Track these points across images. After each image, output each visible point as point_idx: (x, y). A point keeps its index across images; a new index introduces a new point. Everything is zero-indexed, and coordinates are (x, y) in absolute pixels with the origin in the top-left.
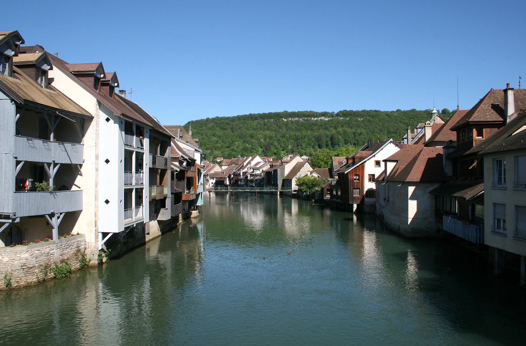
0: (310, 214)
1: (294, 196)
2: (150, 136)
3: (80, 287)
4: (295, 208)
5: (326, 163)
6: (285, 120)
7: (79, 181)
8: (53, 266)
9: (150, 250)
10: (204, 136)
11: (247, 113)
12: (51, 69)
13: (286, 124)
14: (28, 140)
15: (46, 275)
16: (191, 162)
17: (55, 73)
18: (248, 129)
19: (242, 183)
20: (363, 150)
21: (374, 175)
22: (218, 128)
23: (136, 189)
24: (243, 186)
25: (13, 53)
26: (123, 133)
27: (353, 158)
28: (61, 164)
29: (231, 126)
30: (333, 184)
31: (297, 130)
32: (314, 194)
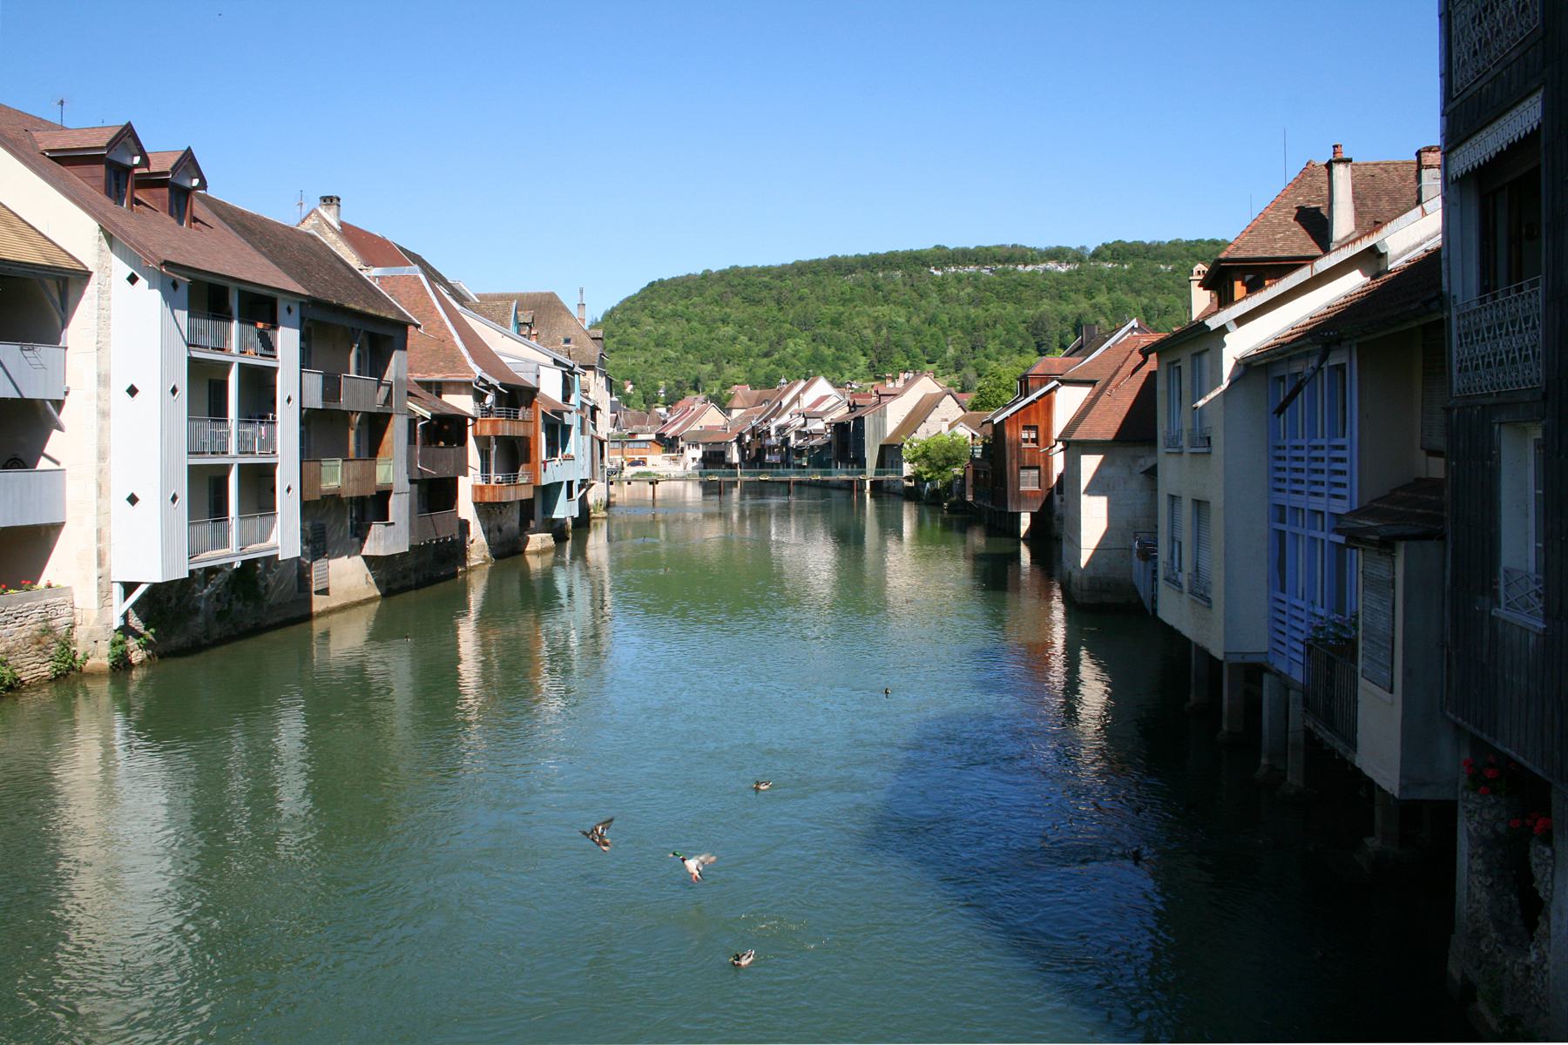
1: (912, 495)
2: (302, 319)
3: (56, 724)
6: (939, 273)
7: (55, 444)
9: (333, 637)
10: (695, 324)
11: (825, 255)
13: (941, 285)
18: (826, 300)
19: (775, 459)
22: (736, 299)
23: (240, 466)
24: (776, 465)
26: (183, 316)
29: (774, 292)
31: (973, 302)
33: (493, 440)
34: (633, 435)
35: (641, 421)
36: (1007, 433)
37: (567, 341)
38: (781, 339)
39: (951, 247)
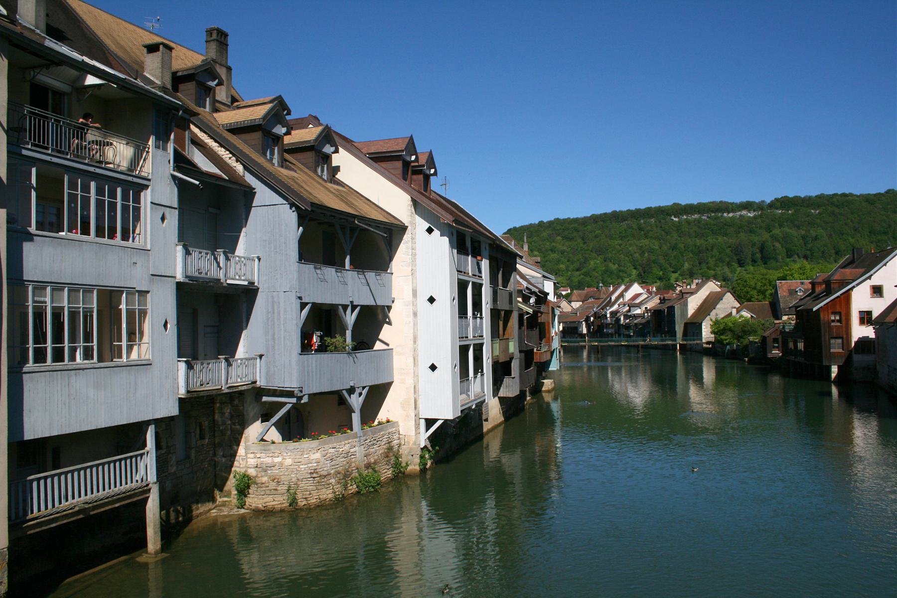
0: (740, 385)
4: (708, 373)
5: (762, 292)
6: (676, 219)
7: (386, 333)
8: (355, 474)
11: (609, 210)
12: (337, 151)
13: (678, 226)
14: (315, 268)
15: (345, 487)
16: (542, 298)
17: (342, 158)
20: (844, 266)
21: (869, 313)
22: (559, 238)
23: (474, 345)
25: (284, 130)
26: (455, 251)
27: (828, 283)
28: (362, 306)
29: (580, 233)
30: (787, 330)
32: (746, 347)
36: (822, 316)
38: (586, 260)
39: (683, 204)
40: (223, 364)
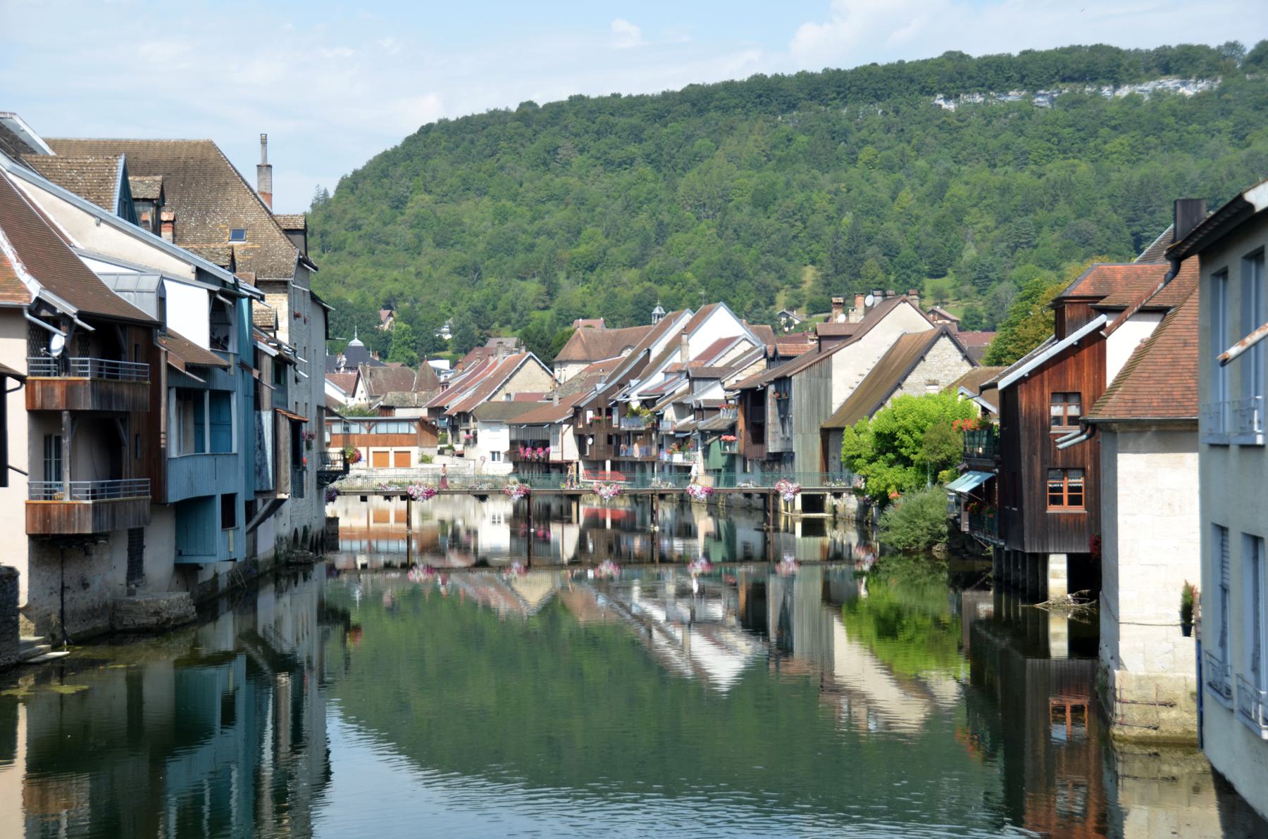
6: (951, 106)
33: (65, 418)
34: (388, 409)
35: (403, 384)
37: (238, 234)
38: (662, 231)
40: (370, 591)
